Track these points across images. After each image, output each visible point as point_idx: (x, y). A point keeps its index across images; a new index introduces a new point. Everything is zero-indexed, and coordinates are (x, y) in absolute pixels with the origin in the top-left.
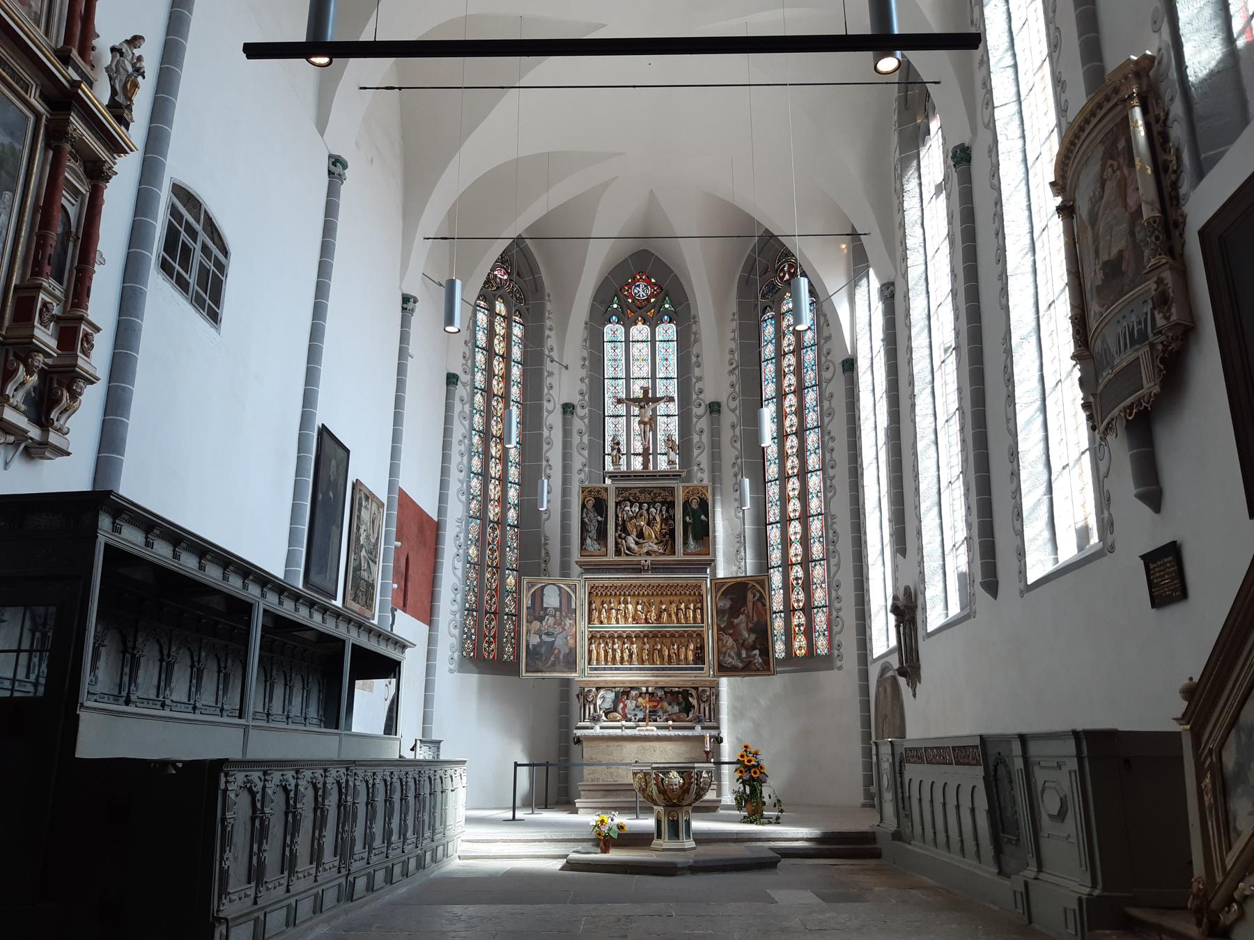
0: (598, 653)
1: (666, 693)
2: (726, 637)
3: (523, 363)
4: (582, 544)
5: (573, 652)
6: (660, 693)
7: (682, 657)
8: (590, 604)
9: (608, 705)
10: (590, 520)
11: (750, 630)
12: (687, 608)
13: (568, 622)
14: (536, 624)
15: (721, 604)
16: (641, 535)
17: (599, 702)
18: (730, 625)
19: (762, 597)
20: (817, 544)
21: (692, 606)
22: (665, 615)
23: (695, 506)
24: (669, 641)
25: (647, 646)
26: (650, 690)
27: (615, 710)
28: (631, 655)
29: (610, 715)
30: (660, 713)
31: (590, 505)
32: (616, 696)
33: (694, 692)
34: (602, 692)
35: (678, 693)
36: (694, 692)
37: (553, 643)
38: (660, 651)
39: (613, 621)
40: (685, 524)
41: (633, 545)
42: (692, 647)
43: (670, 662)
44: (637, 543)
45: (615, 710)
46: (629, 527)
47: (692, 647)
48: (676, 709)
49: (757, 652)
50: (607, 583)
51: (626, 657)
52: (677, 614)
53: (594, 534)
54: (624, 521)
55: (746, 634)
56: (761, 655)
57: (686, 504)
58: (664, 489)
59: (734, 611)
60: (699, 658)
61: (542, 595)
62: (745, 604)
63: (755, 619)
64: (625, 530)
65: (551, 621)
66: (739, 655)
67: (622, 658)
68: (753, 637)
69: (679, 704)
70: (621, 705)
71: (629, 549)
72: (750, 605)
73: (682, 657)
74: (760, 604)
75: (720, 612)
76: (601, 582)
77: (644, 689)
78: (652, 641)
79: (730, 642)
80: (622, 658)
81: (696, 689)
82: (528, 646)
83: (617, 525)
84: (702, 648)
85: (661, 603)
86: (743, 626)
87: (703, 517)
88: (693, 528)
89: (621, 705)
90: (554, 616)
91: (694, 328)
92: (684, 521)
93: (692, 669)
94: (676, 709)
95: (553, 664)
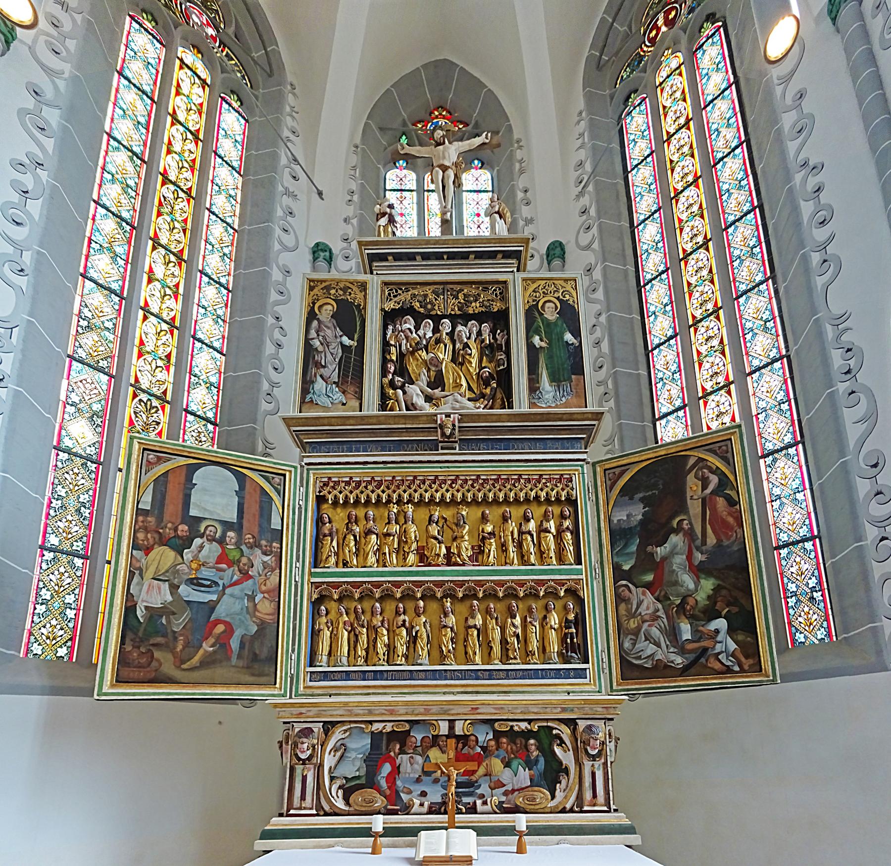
0: (334, 637)
1: (498, 735)
2: (636, 593)
3: (244, 171)
4: (305, 391)
5: (268, 631)
6: (484, 736)
7: (534, 645)
8: (319, 521)
9: (353, 768)
10: (326, 343)
11: (698, 571)
12: (542, 530)
13: (259, 559)
14: (164, 556)
15: (620, 516)
16: (438, 382)
17: (329, 761)
18: (646, 561)
19: (724, 483)
20: (774, 418)
21: (552, 525)
22: (492, 546)
23: (551, 314)
24: (501, 606)
25: (451, 620)
26: (459, 730)
27: (370, 782)
28: (413, 640)
29: (357, 798)
30: (484, 789)
31: (326, 312)
32: (375, 745)
33: (565, 732)
34: (337, 735)
35: (527, 734)
36: (565, 732)
37: (211, 607)
38: (482, 631)
39: (372, 559)
40: (533, 352)
41: (420, 401)
42: (554, 619)
43: (505, 657)
44: (428, 399)
45: (370, 782)
46: (412, 366)
47: (554, 619)
48: (524, 776)
49: (721, 624)
50: (357, 473)
51: (401, 649)
52: (520, 545)
53: (332, 370)
54: (401, 356)
55: (687, 581)
56: (731, 631)
57: (532, 313)
58: (485, 285)
59: (654, 530)
60: (575, 646)
61: (189, 485)
62: (682, 508)
63: (711, 540)
64: (402, 371)
65: (210, 551)
66: (673, 634)
67: (391, 648)
68: (708, 584)
69: (530, 764)
70: (387, 768)
71: (410, 406)
72: (694, 508)
73: (534, 645)
74: (721, 502)
75: (619, 535)
76: (345, 473)
77: (444, 728)
78: (462, 608)
79: (648, 603)
80: (391, 648)
81: (571, 723)
82: (130, 610)
83: (385, 361)
84: (580, 621)
85: (484, 519)
86: (679, 560)
87: (568, 337)
88: (550, 357)
89: (387, 768)
90: (221, 542)
91: (519, 154)
92: (530, 346)
93: (558, 674)
94: (524, 776)
95: (208, 662)
